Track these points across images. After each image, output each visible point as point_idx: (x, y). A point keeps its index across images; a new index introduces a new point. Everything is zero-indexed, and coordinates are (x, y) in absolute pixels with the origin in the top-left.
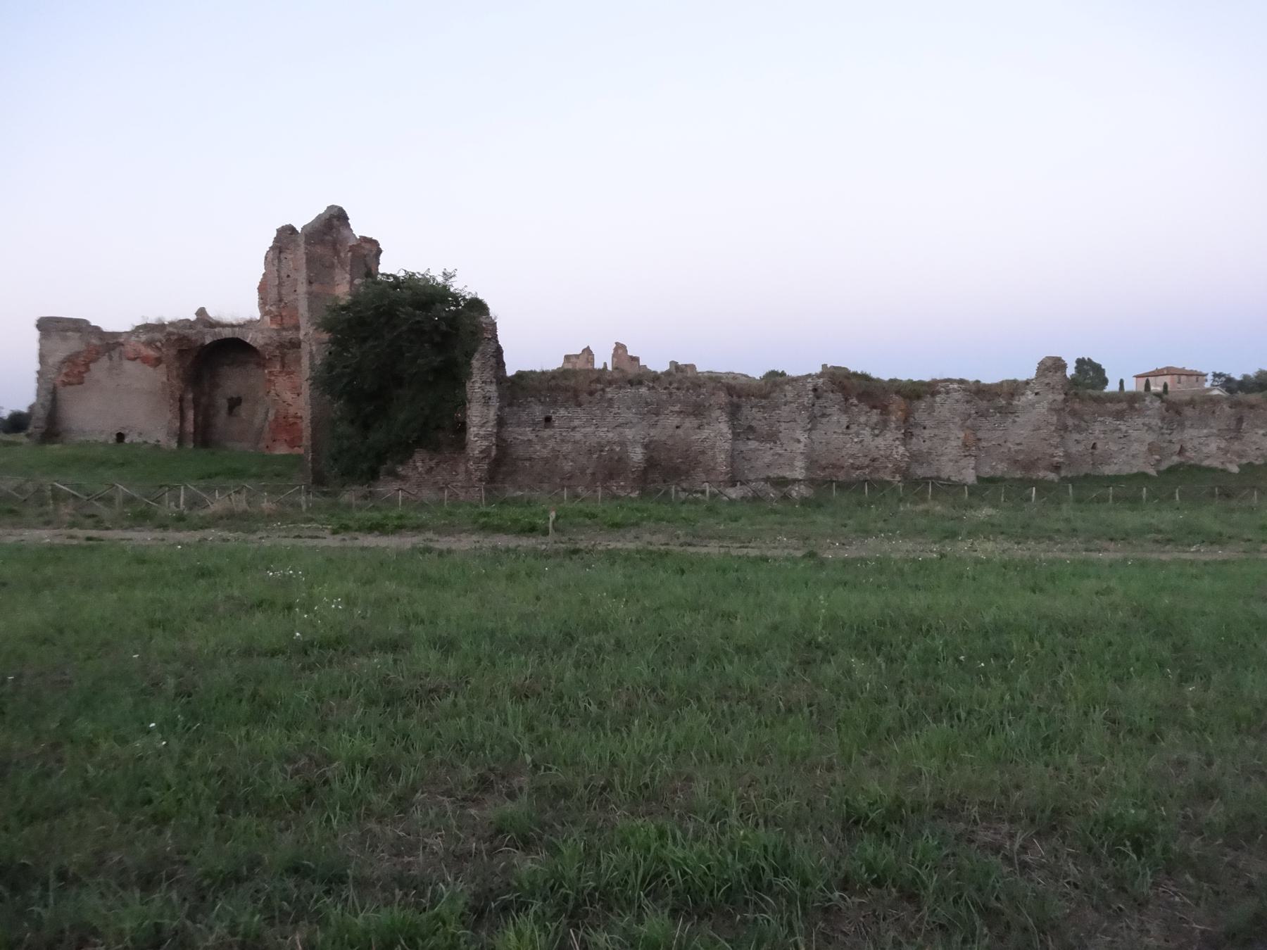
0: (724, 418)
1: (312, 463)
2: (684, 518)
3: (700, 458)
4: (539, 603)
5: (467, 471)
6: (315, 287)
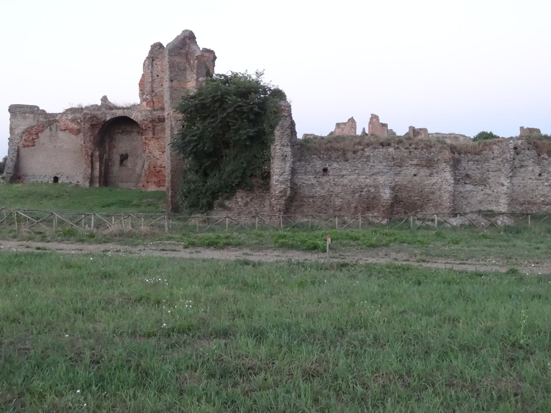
0: (448, 169)
1: (171, 198)
3: (431, 197)
4: (321, 305)
6: (175, 83)
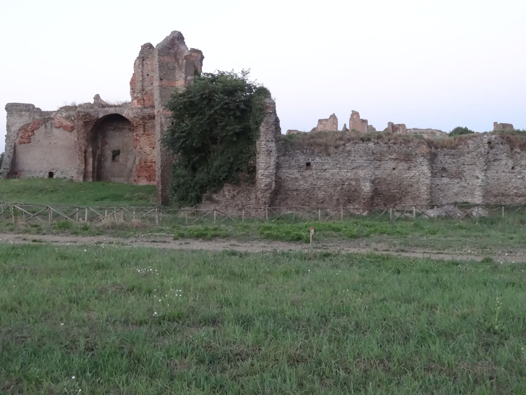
0: (426, 162)
2: (398, 232)
3: (409, 189)
5: (256, 197)
6: (164, 82)
